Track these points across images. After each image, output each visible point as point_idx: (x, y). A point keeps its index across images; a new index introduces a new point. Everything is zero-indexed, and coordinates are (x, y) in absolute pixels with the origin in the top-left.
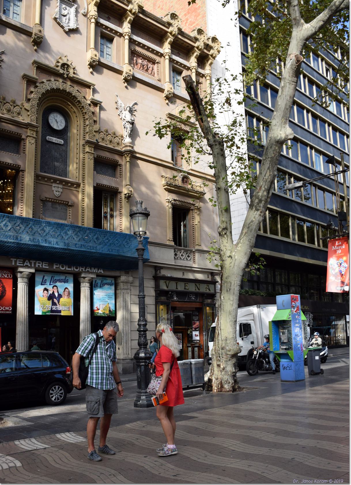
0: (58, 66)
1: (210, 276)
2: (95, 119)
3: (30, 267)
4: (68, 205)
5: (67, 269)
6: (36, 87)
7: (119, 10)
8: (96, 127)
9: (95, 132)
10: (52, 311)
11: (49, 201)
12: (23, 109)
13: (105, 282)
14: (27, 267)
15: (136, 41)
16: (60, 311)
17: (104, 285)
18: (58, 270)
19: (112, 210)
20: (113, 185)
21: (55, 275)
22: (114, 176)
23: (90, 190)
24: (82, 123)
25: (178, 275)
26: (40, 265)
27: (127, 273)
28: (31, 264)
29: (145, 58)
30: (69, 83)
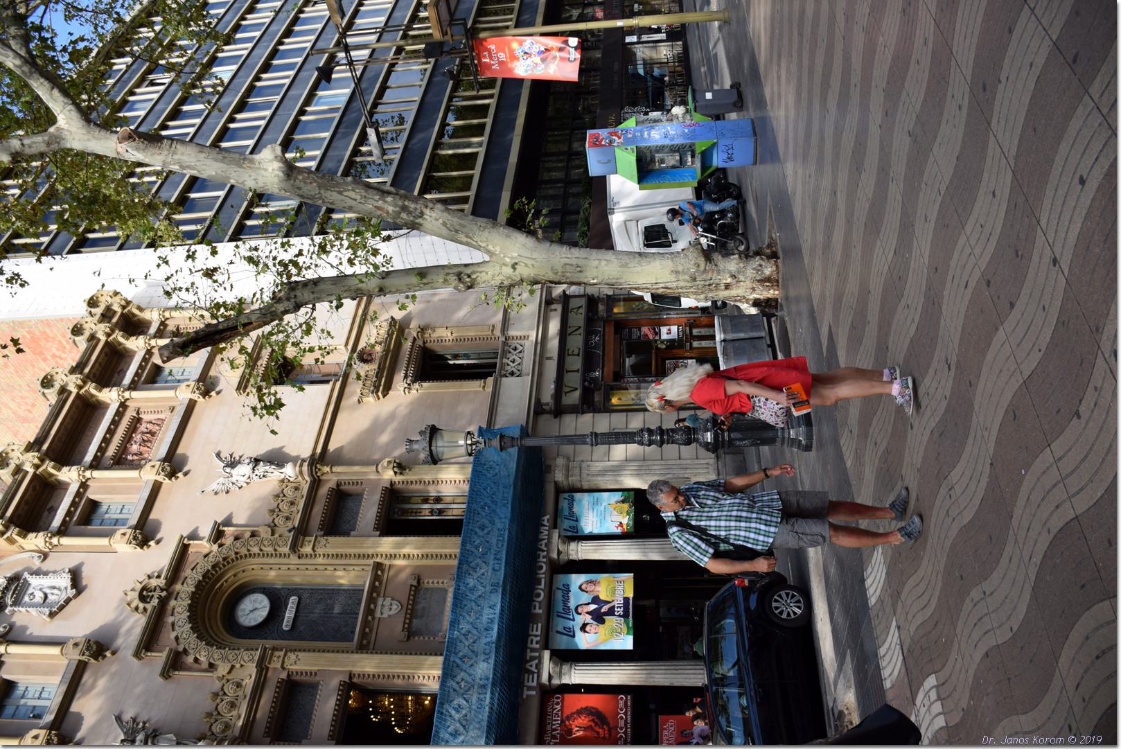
0: (145, 609)
1: (553, 307)
2: (248, 535)
3: (540, 659)
4: (417, 587)
5: (542, 586)
6: (185, 651)
7: (34, 489)
8: (264, 532)
9: (273, 534)
10: (625, 615)
11: (410, 624)
12: (229, 677)
13: (566, 512)
14: (539, 666)
15: (64, 520)
16: (626, 599)
17: (572, 513)
18: (544, 604)
19: (426, 501)
20: (377, 497)
21: (556, 608)
22: (358, 497)
23: (388, 544)
24: (256, 560)
25: (551, 368)
26: (535, 639)
27: (549, 469)
28: (533, 658)
29: (128, 439)
30: (178, 587)
